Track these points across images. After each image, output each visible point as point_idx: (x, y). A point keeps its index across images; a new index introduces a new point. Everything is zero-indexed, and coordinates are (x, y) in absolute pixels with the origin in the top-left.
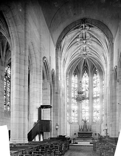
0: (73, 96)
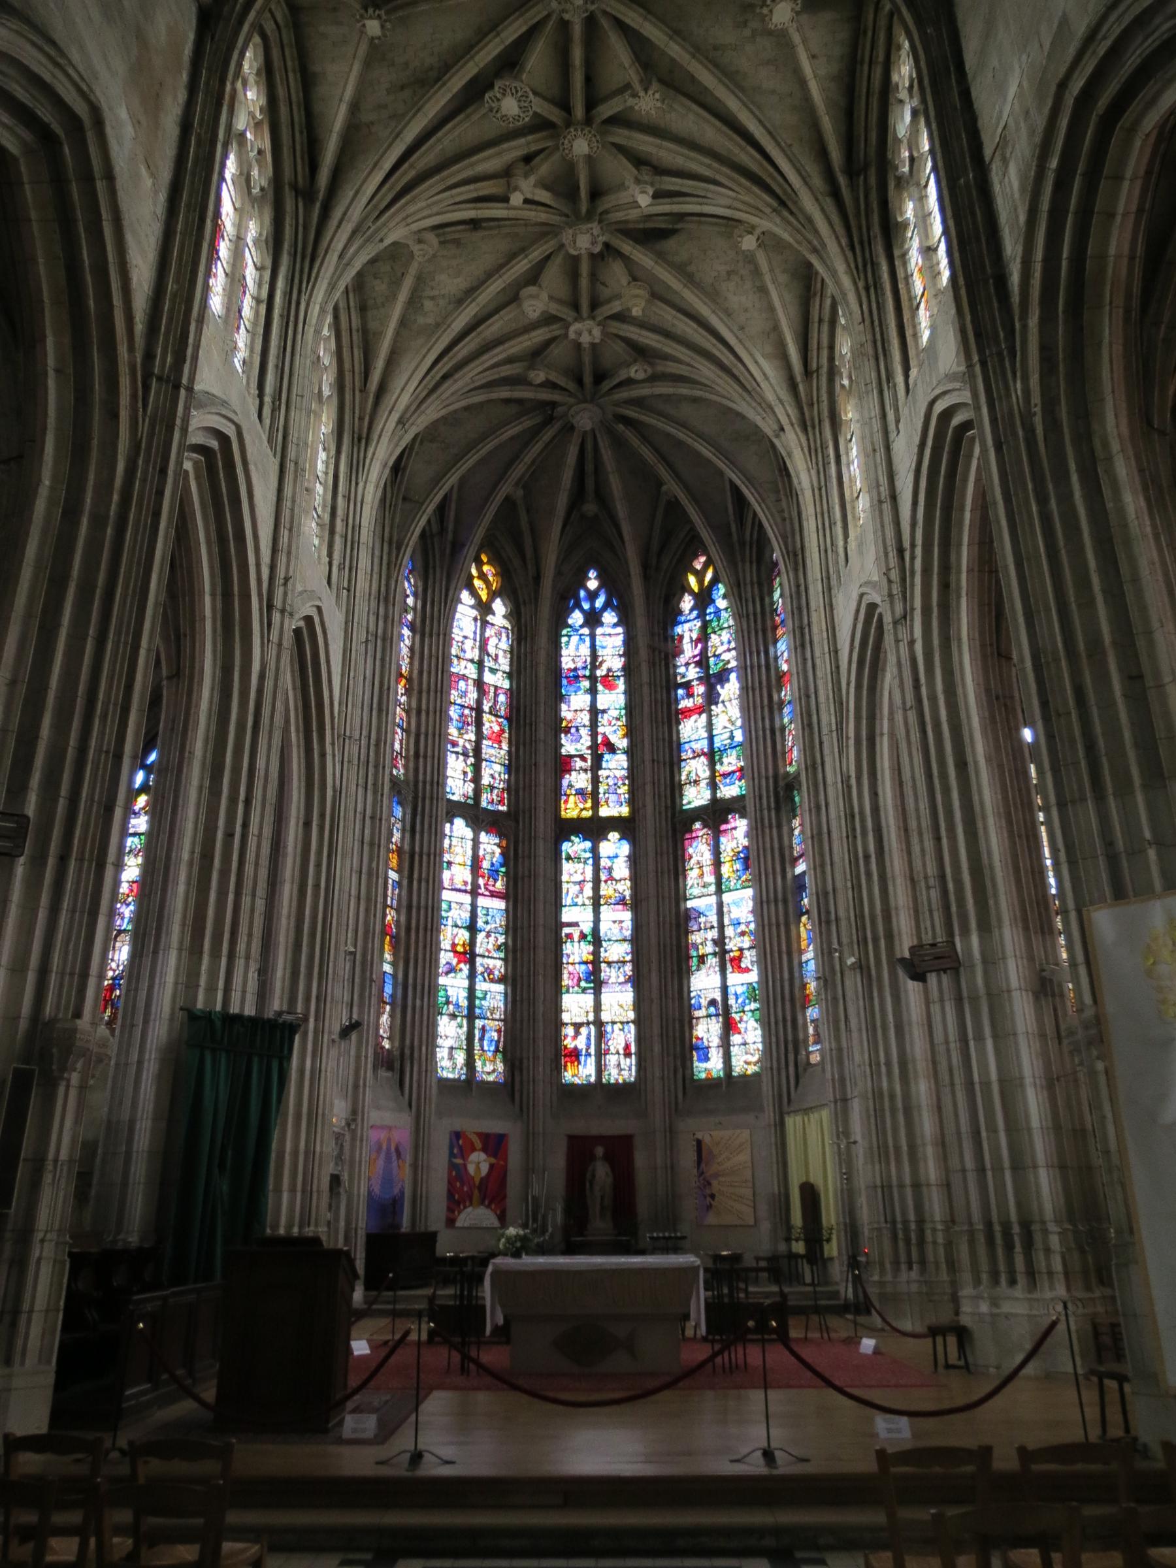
0: (457, 786)
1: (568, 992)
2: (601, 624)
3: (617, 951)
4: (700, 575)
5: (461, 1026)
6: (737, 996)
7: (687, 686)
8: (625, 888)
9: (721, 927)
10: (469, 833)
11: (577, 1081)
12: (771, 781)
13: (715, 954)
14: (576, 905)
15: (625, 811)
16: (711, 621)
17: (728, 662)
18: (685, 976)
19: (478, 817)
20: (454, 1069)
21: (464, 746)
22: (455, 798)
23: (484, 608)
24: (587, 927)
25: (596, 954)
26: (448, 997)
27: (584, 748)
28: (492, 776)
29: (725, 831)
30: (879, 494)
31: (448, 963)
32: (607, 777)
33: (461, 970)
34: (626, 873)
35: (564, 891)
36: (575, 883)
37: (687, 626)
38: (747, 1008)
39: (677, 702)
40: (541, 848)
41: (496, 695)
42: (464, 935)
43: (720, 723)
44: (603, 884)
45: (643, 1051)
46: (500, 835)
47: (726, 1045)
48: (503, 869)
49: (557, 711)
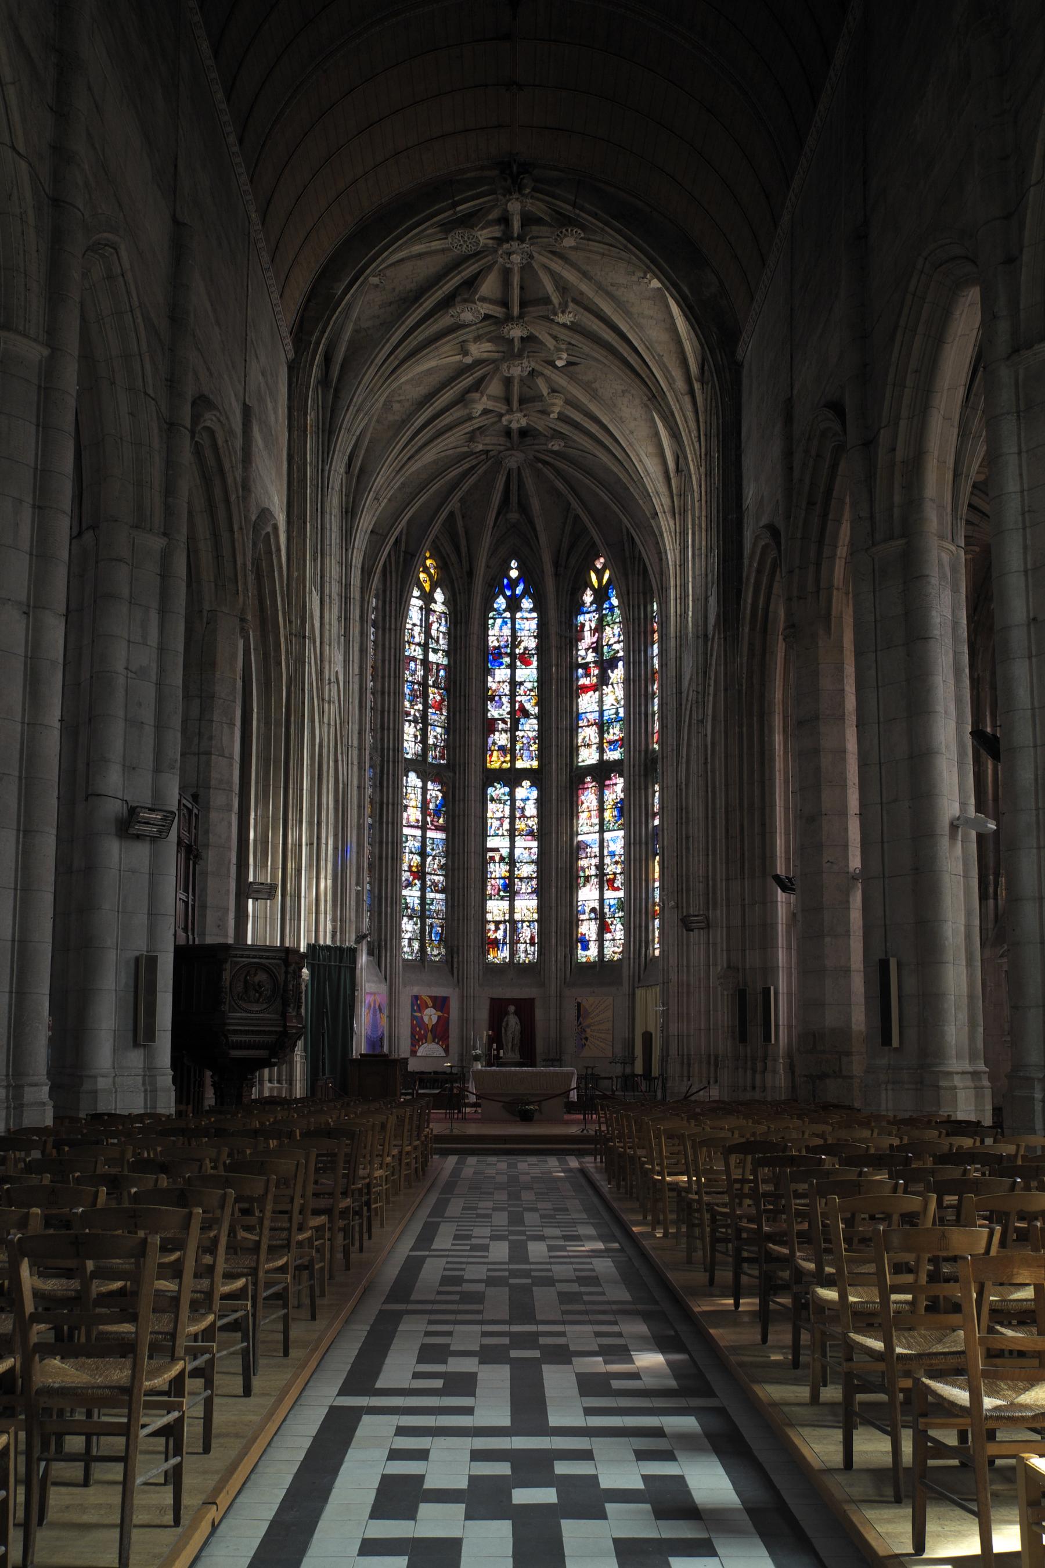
0: (411, 748)
1: (491, 899)
2: (520, 609)
3: (527, 870)
4: (600, 574)
5: (416, 924)
6: (610, 906)
7: (586, 666)
8: (533, 823)
9: (602, 857)
10: (419, 784)
11: (496, 961)
12: (643, 753)
13: (596, 876)
14: (497, 835)
15: (535, 764)
16: (606, 615)
17: (618, 652)
18: (575, 890)
19: (421, 766)
20: (412, 953)
21: (415, 715)
22: (409, 756)
23: (428, 598)
24: (505, 852)
25: (511, 871)
26: (407, 904)
27: (505, 713)
28: (435, 737)
29: (609, 785)
30: (697, 631)
31: (406, 880)
32: (523, 737)
33: (416, 884)
34: (534, 812)
35: (489, 825)
36: (497, 819)
37: (588, 616)
38: (616, 915)
39: (578, 679)
40: (473, 794)
41: (438, 671)
42: (417, 859)
43: (609, 700)
44: (517, 820)
45: (542, 941)
46: (441, 783)
47: (601, 940)
48: (444, 809)
49: (486, 682)
